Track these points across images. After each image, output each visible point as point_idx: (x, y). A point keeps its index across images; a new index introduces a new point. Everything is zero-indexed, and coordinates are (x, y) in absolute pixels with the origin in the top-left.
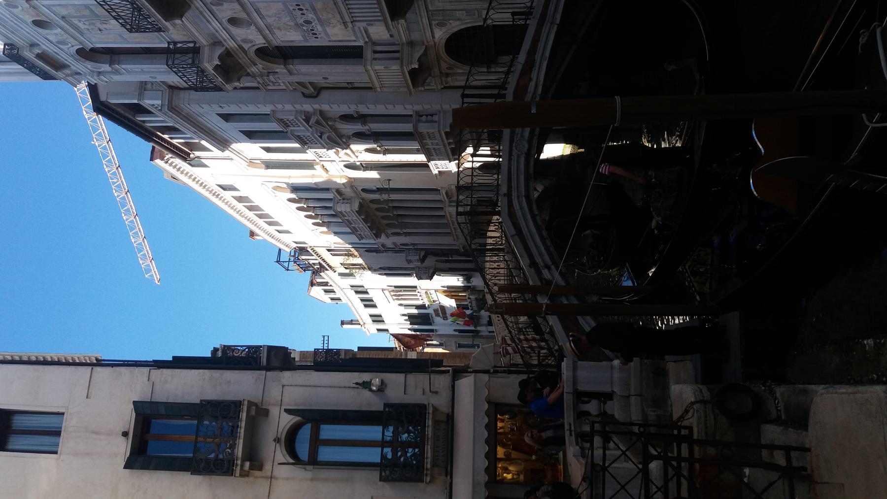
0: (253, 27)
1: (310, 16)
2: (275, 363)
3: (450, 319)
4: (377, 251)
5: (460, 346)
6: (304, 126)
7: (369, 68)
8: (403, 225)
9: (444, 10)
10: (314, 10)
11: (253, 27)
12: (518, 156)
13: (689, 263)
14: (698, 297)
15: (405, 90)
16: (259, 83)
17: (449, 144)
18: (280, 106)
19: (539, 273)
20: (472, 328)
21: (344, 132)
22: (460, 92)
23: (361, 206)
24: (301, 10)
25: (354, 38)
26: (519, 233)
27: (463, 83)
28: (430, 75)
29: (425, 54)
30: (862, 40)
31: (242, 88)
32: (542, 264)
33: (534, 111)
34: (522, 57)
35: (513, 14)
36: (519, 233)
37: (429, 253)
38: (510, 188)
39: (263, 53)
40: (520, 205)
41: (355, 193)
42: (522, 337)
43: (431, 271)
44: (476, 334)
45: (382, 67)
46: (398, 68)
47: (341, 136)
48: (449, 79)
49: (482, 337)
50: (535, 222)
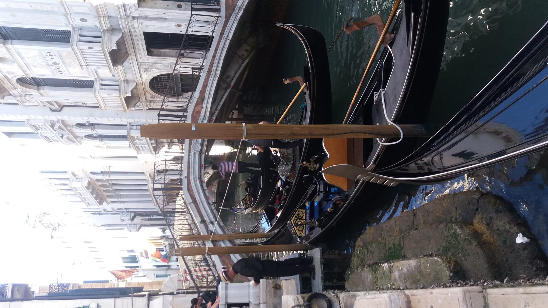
0: (15, 64)
1: (57, 60)
2: (17, 295)
3: (151, 258)
4: (100, 214)
5: (157, 276)
6: (50, 130)
7: (97, 94)
8: (120, 196)
9: (148, 63)
10: (60, 56)
11: (15, 64)
12: (194, 153)
13: (293, 219)
14: (298, 239)
15: (122, 109)
16: (18, 100)
17: (152, 144)
18: (33, 117)
19: (207, 227)
20: (166, 264)
21: (78, 134)
22: (157, 112)
23: (89, 183)
24: (51, 56)
25: (88, 76)
26: (194, 201)
27: (159, 107)
28: (139, 101)
29: (136, 88)
30: (375, 98)
31: (5, 104)
32: (209, 221)
33: (194, 129)
34: (197, 94)
35: (193, 69)
36: (194, 201)
37: (137, 214)
38: (189, 173)
39: (21, 81)
40: (195, 184)
41: (86, 175)
42: (197, 269)
43: (138, 226)
44: (168, 267)
45: (106, 95)
46: (118, 95)
47: (76, 137)
48: (152, 104)
49: (172, 269)
50: (205, 194)
